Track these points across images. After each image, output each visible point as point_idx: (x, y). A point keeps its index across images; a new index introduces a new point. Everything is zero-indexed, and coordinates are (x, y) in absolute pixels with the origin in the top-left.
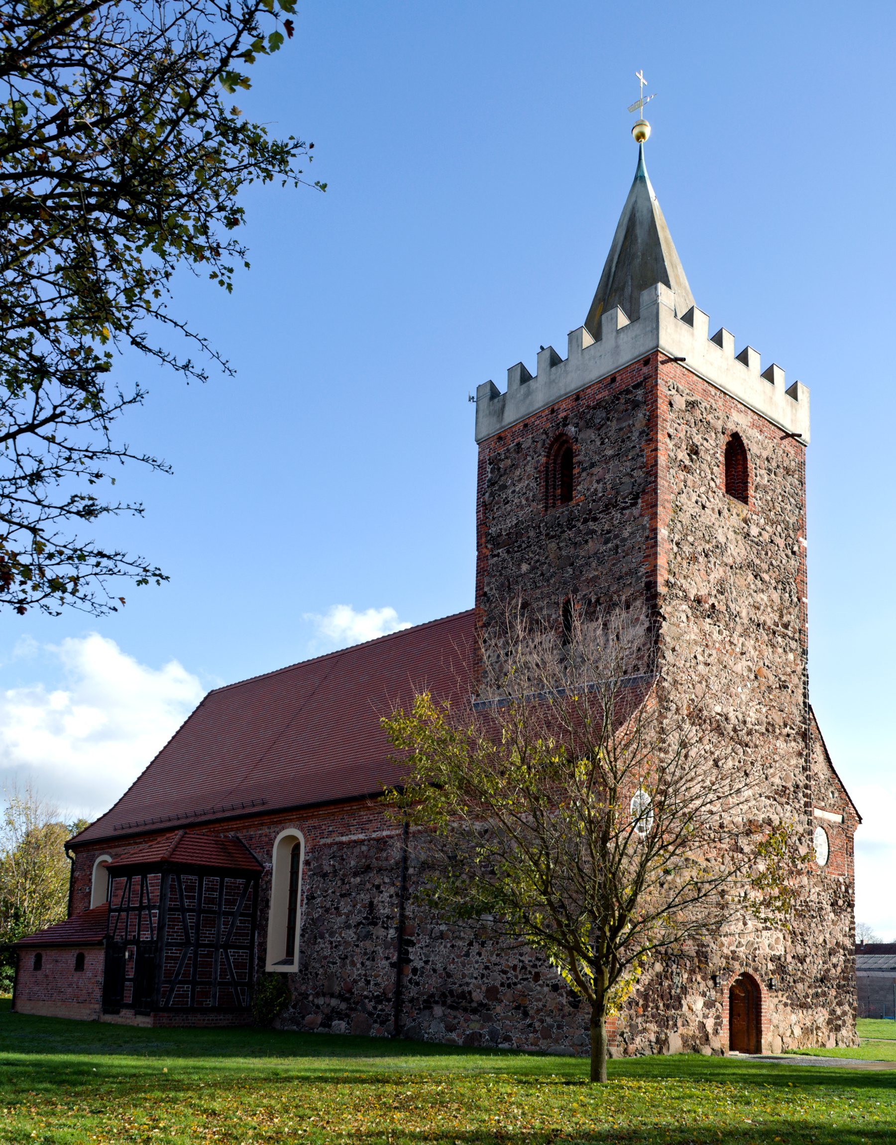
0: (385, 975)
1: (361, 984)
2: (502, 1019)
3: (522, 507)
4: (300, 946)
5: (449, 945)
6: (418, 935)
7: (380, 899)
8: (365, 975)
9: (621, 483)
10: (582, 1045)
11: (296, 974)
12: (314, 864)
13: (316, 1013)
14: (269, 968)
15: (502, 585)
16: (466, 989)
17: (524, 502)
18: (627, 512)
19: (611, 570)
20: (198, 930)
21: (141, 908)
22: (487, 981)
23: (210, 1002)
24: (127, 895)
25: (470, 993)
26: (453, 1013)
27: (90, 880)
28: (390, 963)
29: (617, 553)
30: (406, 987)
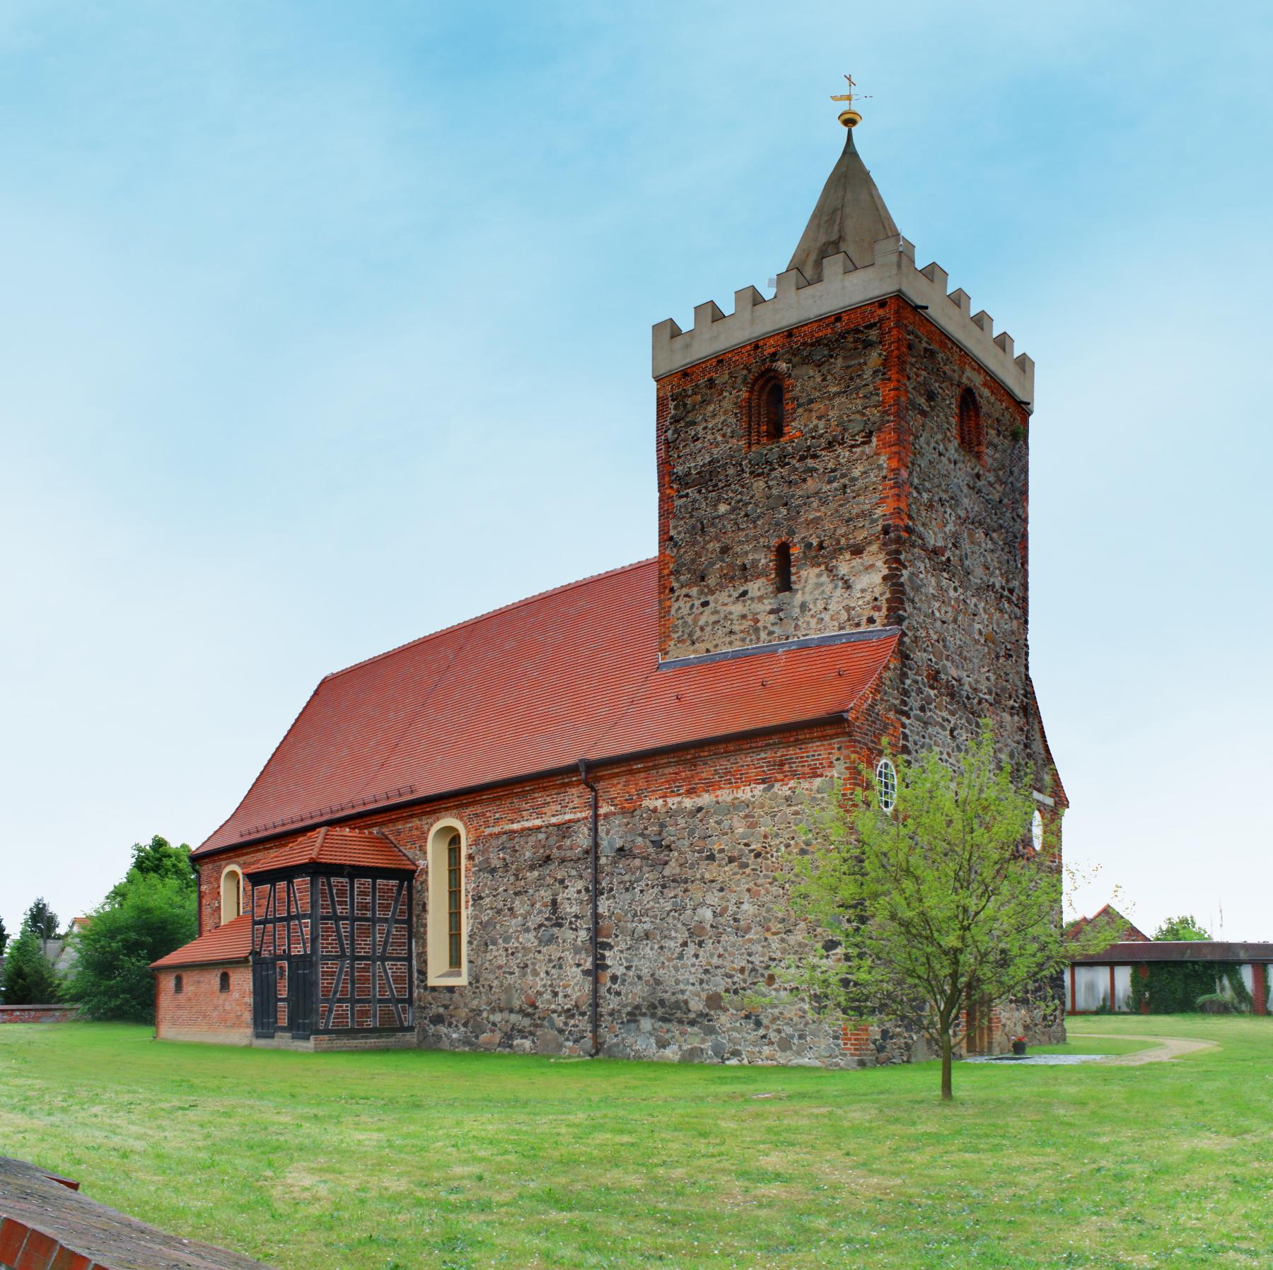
0: (576, 984)
1: (548, 996)
2: (728, 1031)
3: (717, 445)
4: (468, 955)
5: (656, 947)
6: (617, 936)
7: (565, 895)
8: (551, 985)
9: (850, 421)
10: (830, 1056)
11: (465, 987)
12: (479, 859)
13: (493, 1031)
14: (432, 981)
15: (694, 527)
16: (680, 997)
17: (719, 438)
18: (858, 450)
19: (837, 511)
20: (352, 944)
21: (289, 918)
22: (707, 987)
23: (370, 1023)
24: (271, 905)
25: (686, 1002)
26: (666, 1026)
27: (219, 893)
28: (583, 971)
29: (845, 493)
30: (604, 998)
